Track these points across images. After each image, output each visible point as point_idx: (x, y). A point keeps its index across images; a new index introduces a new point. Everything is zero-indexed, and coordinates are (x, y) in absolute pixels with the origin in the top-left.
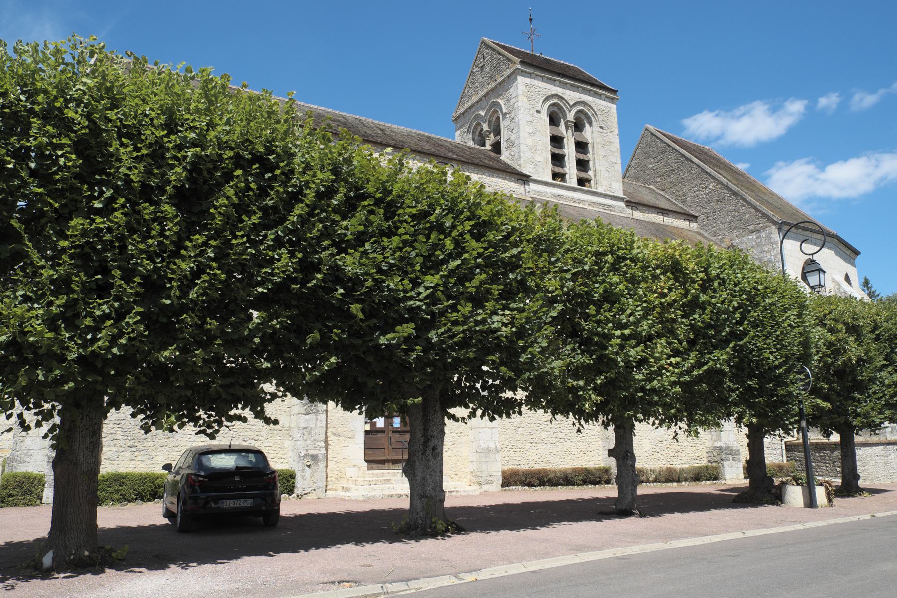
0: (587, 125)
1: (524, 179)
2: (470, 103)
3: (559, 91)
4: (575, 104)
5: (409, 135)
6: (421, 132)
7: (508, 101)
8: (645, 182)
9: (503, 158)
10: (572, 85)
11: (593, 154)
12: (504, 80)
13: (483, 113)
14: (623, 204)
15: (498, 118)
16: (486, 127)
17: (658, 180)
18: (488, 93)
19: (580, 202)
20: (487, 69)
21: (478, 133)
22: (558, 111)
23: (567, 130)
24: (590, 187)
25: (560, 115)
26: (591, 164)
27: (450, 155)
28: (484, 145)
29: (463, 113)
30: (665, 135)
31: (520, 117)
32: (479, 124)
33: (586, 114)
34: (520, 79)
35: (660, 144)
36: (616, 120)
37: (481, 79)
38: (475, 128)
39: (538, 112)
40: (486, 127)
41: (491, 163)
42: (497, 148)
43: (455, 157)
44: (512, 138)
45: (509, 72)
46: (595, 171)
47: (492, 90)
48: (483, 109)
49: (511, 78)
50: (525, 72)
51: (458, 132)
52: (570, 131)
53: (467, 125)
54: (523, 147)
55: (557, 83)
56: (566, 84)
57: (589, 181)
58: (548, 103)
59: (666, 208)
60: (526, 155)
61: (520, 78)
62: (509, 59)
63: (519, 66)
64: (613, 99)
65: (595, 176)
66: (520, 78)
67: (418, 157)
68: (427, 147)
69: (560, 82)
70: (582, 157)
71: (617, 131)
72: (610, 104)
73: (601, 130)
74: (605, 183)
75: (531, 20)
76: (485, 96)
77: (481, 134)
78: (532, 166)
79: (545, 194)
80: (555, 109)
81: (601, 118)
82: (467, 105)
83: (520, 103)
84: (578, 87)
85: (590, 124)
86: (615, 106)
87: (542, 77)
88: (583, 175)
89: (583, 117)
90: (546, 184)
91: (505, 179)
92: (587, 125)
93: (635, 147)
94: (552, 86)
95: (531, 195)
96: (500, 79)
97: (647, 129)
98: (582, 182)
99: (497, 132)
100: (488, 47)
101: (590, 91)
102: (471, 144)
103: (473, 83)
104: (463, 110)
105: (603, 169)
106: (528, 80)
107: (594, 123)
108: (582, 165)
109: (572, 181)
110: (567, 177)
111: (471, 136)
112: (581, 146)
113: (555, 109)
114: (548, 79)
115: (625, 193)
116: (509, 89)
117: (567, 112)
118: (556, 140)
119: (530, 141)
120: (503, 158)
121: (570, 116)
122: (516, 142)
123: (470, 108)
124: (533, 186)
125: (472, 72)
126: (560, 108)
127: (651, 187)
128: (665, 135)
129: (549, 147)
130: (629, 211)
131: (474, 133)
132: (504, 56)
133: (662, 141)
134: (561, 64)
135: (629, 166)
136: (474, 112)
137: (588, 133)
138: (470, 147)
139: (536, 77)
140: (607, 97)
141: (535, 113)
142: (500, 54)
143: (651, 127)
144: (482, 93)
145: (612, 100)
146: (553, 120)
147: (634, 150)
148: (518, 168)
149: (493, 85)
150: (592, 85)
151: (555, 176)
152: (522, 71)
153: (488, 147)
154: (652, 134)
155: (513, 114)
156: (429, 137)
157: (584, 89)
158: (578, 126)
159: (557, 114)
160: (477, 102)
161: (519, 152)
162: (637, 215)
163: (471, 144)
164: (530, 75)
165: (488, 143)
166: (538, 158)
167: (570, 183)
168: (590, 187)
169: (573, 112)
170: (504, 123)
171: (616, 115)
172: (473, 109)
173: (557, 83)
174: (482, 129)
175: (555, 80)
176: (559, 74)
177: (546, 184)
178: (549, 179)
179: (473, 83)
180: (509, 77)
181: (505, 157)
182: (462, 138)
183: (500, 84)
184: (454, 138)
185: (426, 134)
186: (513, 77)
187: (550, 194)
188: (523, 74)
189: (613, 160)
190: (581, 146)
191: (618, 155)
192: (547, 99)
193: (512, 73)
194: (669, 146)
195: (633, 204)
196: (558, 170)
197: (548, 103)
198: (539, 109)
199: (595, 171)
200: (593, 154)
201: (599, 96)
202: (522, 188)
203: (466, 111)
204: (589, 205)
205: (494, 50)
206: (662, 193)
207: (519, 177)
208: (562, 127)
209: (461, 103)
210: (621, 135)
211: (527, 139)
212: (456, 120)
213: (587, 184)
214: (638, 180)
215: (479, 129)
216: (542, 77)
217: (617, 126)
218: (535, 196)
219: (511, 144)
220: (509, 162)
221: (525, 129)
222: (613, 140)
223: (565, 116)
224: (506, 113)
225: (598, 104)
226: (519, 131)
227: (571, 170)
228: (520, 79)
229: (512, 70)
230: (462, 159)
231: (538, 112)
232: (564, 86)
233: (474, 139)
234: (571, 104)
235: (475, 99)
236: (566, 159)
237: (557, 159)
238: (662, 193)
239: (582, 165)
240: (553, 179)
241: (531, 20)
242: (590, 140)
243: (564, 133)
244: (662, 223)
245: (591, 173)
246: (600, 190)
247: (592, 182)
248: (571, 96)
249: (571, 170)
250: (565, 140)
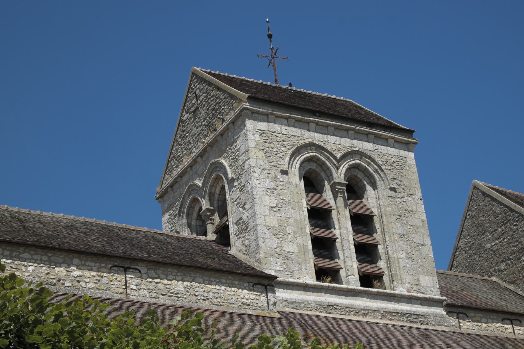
0: (369, 188)
1: (266, 283)
2: (179, 170)
3: (317, 138)
4: (344, 157)
5: (71, 226)
6: (93, 220)
7: (235, 159)
8: (484, 271)
9: (233, 251)
10: (336, 128)
11: (383, 233)
12: (227, 129)
13: (199, 183)
14: (440, 311)
15: (223, 188)
16: (205, 204)
17: (503, 266)
18: (204, 151)
19: (367, 312)
20: (202, 113)
21: (195, 215)
22: (318, 170)
23: (335, 198)
24: (383, 286)
25: (323, 175)
26: (381, 248)
27: (135, 253)
28: (205, 234)
29: (171, 186)
30: (504, 194)
31: (255, 182)
32: (195, 201)
33: (365, 171)
34: (251, 126)
35: (499, 210)
36: (416, 176)
37: (194, 131)
38: (191, 207)
39: (285, 172)
40: (205, 204)
41: (209, 261)
42: (223, 233)
43: (143, 255)
44: (245, 217)
45: (232, 115)
46: (388, 260)
47: (211, 145)
48: (200, 176)
49: (237, 124)
50: (258, 113)
51: (166, 217)
52: (340, 200)
53: (178, 204)
54: (261, 230)
55: (313, 126)
56: (327, 126)
57: (379, 277)
58: (300, 159)
59: (517, 310)
60: (268, 243)
61: (250, 124)
62: (232, 96)
63: (247, 105)
64: (408, 143)
65: (389, 268)
66: (250, 124)
67: (76, 261)
68: (97, 243)
69: (317, 124)
70: (364, 239)
71: (418, 194)
72: (403, 153)
73: (392, 193)
74: (408, 278)
75: (270, 36)
76: (201, 155)
77: (199, 217)
78: (280, 261)
79: (305, 304)
80: (314, 166)
81: (391, 175)
82: (175, 173)
83: (252, 162)
84: (347, 130)
85: (374, 186)
86: (412, 155)
87: (287, 118)
88: (369, 268)
89: (360, 175)
90: (305, 288)
91: (231, 285)
92: (369, 188)
93: (461, 217)
94: (304, 132)
95: (280, 307)
96: (220, 128)
97: (475, 188)
98: (367, 280)
99: (223, 212)
100: (202, 80)
101: (368, 134)
102: (186, 233)
103: (183, 137)
104: (169, 180)
105: (402, 255)
106: (263, 126)
107: (379, 183)
108: (366, 252)
109: (351, 279)
110: (342, 273)
111: (184, 221)
112: (362, 222)
113: (314, 166)
114: (297, 120)
115: (443, 291)
116: (235, 141)
117: (334, 171)
118: (319, 216)
119: (273, 220)
120: (233, 251)
121: (339, 175)
122: (251, 224)
123: (181, 176)
124: (281, 294)
125: (181, 121)
126: (322, 164)
127: (494, 279)
128: (497, 190)
129: (308, 229)
130: (453, 321)
131: (189, 215)
132: (224, 91)
133: (501, 203)
134: (323, 98)
135: (457, 249)
136: (186, 183)
137: (372, 200)
138: (185, 240)
139: (277, 119)
140: (397, 141)
141: (279, 176)
142: (219, 89)
143: (481, 184)
144: (196, 151)
145: (407, 146)
146: (312, 183)
147: (460, 223)
148: (256, 265)
149: (211, 137)
150: (371, 125)
151: (321, 273)
152: (253, 112)
153: (211, 236)
154: (484, 194)
155: (243, 180)
156: (107, 227)
157: (358, 132)
158: (353, 190)
159: (318, 174)
160: (191, 166)
161: (256, 240)
162: (468, 326)
163: (186, 233)
164: (266, 118)
165: (210, 228)
166: (289, 247)
167: (348, 282)
168: (383, 286)
169: (343, 169)
170: (231, 195)
171: (415, 169)
172: (185, 178)
173: (313, 126)
174: (201, 208)
175: (308, 122)
176: (313, 113)
177: (305, 288)
178: (311, 280)
179: (183, 137)
180: (233, 122)
181: (236, 249)
182: (170, 225)
183: (222, 134)
184: (161, 229)
185: (103, 222)
186: (239, 122)
187: (314, 302)
188: (255, 116)
189: (417, 239)
190: (362, 222)
191: (425, 231)
192: (297, 151)
193: (238, 117)
194: (512, 210)
195: (458, 309)
196: (326, 263)
197: (300, 159)
198: (285, 168)
199: (388, 260)
200: (383, 233)
201: (385, 141)
202: (263, 298)
203: (175, 182)
204: (383, 317)
205: (210, 84)
206: (511, 287)
207: (256, 280)
208: (328, 194)
209: (167, 170)
210: (425, 198)
211: (271, 217)
212: (161, 197)
213: (375, 282)
214: (472, 270)
215: (197, 209)
216: (287, 118)
217: (418, 185)
218: (287, 310)
219: (244, 227)
220: (242, 257)
221: (264, 202)
222: (414, 208)
223: (330, 177)
224: (233, 179)
225: (384, 153)
226: (253, 206)
227: (348, 262)
228: (251, 126)
229: (237, 110)
230: (155, 258)
231: (285, 172)
232: (325, 130)
233: (189, 226)
234: (338, 156)
235: (187, 161)
236: (338, 244)
237: (323, 246)
238: (511, 287)
239: (366, 252)
240: (318, 278)
241: (270, 36)
242: (375, 211)
243: (332, 203)
244: (511, 336)
245: (382, 264)
246: (400, 290)
247: (386, 278)
248: (337, 144)
249: (348, 262)
250: (334, 214)
